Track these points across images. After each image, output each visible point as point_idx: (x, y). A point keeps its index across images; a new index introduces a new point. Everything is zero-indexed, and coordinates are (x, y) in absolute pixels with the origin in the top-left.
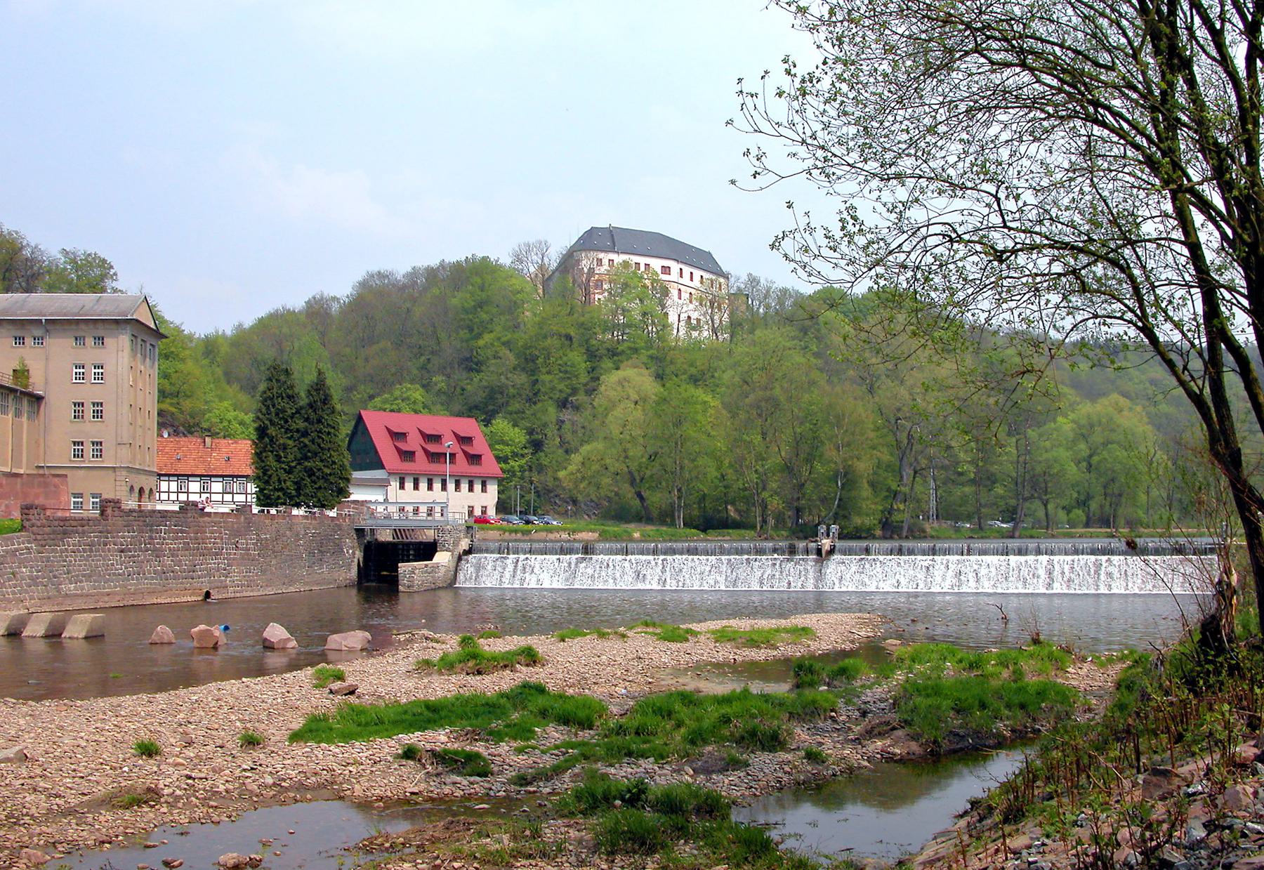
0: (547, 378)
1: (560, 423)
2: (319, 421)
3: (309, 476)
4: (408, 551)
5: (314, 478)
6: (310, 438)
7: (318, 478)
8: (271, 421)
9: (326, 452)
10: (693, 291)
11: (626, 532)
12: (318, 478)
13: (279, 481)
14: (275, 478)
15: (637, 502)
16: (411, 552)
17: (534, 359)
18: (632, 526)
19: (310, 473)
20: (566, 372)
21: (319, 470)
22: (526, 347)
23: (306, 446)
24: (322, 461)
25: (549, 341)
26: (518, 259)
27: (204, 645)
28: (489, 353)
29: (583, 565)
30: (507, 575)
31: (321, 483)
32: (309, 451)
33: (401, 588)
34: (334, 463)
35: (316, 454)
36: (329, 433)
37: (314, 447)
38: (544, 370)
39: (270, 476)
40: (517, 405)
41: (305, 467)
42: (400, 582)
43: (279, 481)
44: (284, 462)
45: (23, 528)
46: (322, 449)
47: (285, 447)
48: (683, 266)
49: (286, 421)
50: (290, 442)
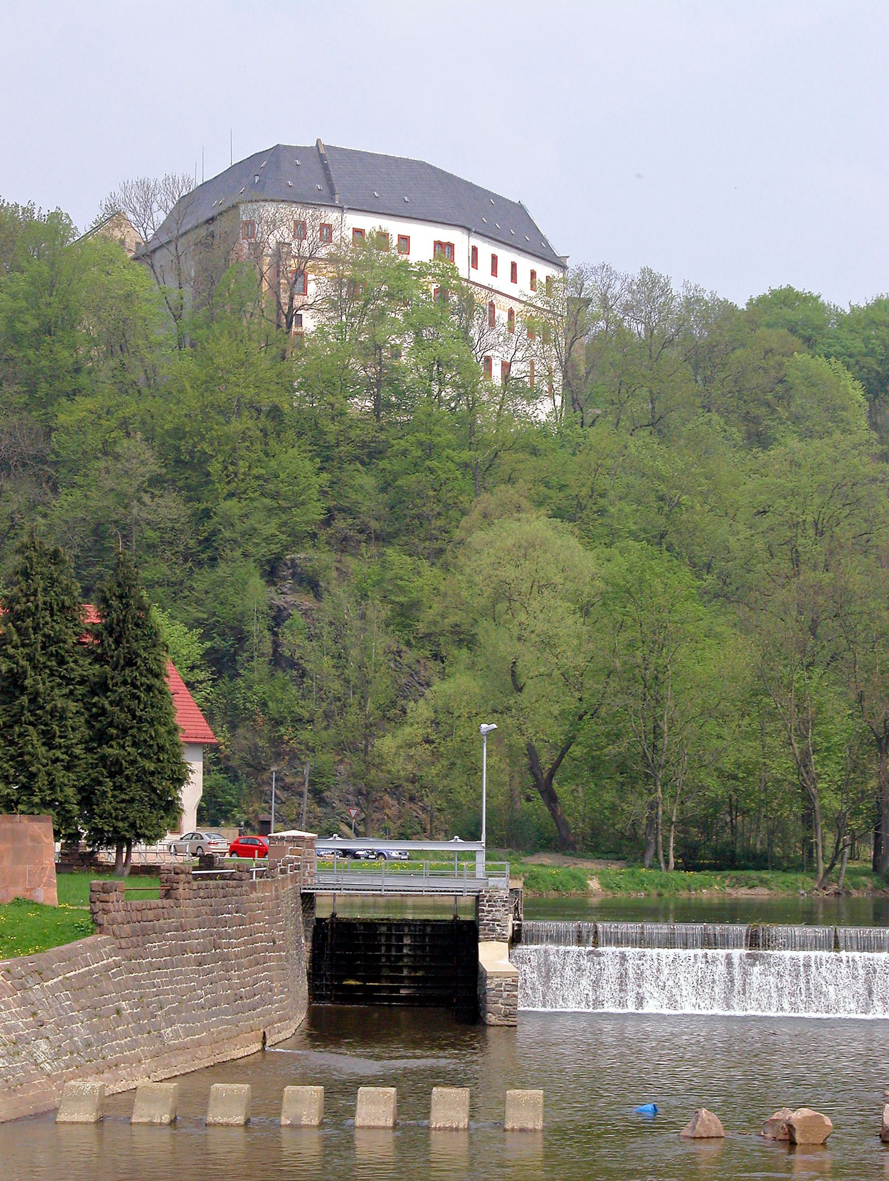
0: (232, 506)
1: (278, 617)
2: (130, 663)
3: (111, 775)
4: (400, 938)
5: (119, 780)
6: (112, 697)
7: (128, 778)
8: (30, 658)
9: (145, 726)
10: (517, 307)
11: (574, 877)
12: (128, 778)
13: (52, 785)
14: (42, 781)
15: (539, 803)
16: (407, 941)
17: (198, 462)
18: (586, 866)
19: (115, 769)
20: (275, 496)
21: (133, 762)
22: (178, 433)
23: (103, 712)
24: (135, 744)
25: (236, 426)
26: (115, 217)
27: (811, 1140)
28: (93, 440)
29: (757, 969)
30: (607, 990)
31: (135, 791)
32: (111, 724)
33: (491, 1018)
34: (161, 748)
35: (124, 731)
36: (149, 688)
37: (122, 717)
38: (222, 489)
39: (32, 776)
40: (164, 568)
41: (103, 758)
42: (490, 1006)
43: (52, 785)
44: (60, 747)
45: (98, 926)
46: (140, 720)
47: (60, 715)
48: (476, 242)
49: (62, 662)
50: (73, 706)
